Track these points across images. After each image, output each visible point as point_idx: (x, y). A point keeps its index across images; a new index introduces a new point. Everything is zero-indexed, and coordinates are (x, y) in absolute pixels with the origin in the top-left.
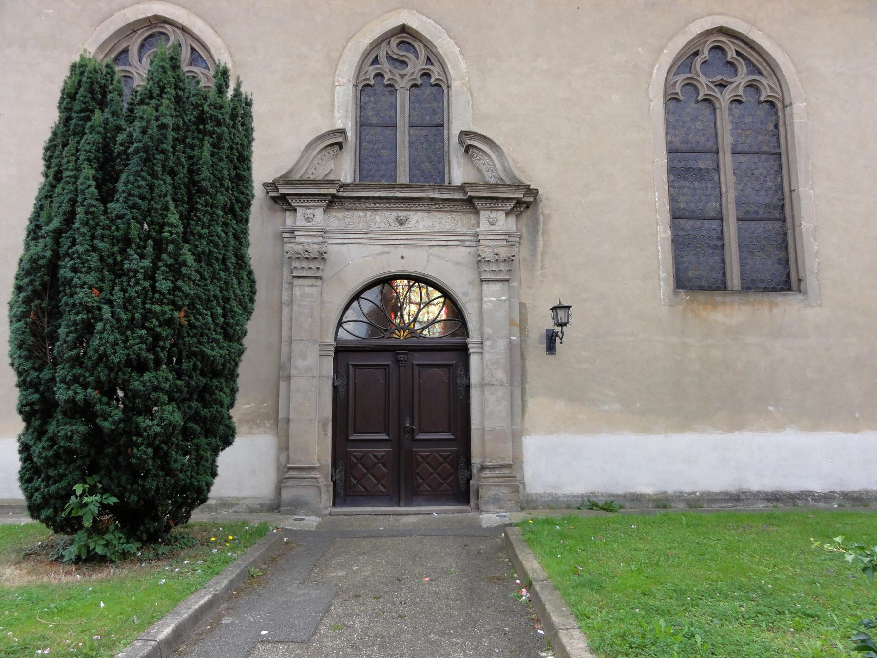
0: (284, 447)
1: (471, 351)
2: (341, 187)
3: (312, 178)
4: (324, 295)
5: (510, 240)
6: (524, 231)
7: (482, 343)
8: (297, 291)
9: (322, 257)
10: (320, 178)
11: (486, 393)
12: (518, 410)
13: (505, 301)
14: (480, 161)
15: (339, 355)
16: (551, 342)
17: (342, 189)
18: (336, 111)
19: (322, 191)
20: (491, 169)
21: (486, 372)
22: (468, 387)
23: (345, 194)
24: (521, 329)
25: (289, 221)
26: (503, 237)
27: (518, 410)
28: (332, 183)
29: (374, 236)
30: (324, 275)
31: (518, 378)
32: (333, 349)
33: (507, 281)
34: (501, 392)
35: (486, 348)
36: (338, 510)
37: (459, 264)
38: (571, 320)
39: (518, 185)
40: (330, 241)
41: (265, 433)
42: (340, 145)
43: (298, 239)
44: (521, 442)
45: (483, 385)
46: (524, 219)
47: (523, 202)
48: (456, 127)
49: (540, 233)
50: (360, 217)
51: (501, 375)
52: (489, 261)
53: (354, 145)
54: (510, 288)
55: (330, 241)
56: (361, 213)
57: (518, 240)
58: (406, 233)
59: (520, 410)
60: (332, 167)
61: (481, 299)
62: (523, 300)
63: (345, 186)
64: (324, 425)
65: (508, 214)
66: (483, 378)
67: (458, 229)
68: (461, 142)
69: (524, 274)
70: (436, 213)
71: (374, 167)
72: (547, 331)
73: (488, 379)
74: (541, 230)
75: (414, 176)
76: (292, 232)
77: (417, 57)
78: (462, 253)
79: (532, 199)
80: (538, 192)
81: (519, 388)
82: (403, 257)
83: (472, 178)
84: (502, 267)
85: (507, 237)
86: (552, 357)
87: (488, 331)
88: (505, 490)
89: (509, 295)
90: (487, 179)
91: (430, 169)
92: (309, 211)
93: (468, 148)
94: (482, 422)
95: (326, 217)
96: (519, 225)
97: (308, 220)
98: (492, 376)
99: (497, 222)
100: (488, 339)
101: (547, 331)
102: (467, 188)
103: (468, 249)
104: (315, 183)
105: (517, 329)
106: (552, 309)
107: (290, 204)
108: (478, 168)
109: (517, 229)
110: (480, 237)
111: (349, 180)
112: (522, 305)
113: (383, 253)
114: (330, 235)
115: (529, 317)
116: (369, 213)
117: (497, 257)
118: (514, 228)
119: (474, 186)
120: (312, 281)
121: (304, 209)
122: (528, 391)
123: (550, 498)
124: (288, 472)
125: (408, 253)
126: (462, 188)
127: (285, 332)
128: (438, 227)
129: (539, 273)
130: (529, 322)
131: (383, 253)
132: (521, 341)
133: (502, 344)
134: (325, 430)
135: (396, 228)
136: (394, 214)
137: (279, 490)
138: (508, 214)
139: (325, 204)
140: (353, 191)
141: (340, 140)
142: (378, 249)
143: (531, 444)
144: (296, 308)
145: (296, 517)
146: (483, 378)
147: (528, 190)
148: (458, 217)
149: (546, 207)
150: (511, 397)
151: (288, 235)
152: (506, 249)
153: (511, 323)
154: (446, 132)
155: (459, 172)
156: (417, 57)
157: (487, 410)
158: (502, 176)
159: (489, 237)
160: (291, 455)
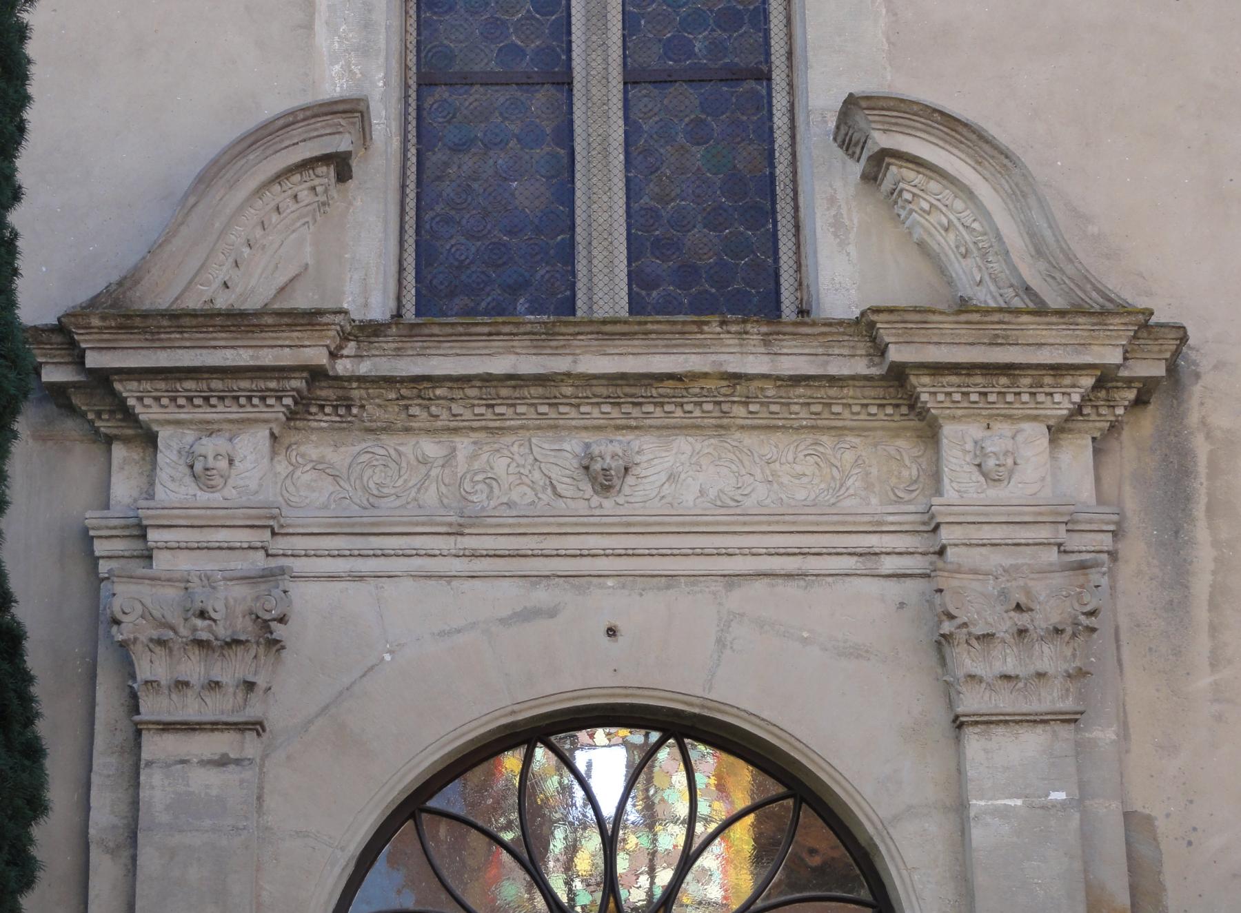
2: (345, 337)
3: (221, 303)
4: (270, 802)
5: (1074, 542)
6: (1131, 504)
9: (267, 634)
10: (252, 304)
13: (1063, 805)
14: (938, 216)
18: (320, 27)
19: (268, 358)
20: (968, 230)
25: (123, 489)
26: (1043, 533)
28: (309, 319)
30: (276, 714)
33: (1071, 719)
37: (857, 653)
39: (1100, 311)
40: (298, 565)
42: (341, 166)
43: (162, 561)
47: (1132, 381)
49: (1200, 510)
50: (424, 461)
52: (987, 638)
53: (395, 165)
54: (1082, 750)
55: (298, 565)
56: (430, 448)
57: (1106, 541)
60: (308, 254)
61: (960, 808)
62: (1138, 806)
63: (369, 332)
67: (848, 504)
68: (848, 138)
74: (1202, 500)
75: (650, 285)
76: (140, 531)
77: (1084, 614)
78: (869, 608)
79: (1159, 370)
80: (1184, 339)
82: (612, 632)
84: (1048, 658)
85: (1062, 535)
89: (1082, 785)
90: (967, 290)
91: (719, 256)
92: (210, 446)
95: (282, 467)
97: (201, 475)
102: (886, 334)
104: (238, 322)
109: (1100, 500)
110: (946, 535)
111: (378, 308)
112: (1136, 824)
114: (300, 543)
115: (1169, 879)
118: (1086, 493)
119: (915, 316)
121: (190, 436)
125: (638, 610)
126: (866, 328)
128: (759, 496)
135: (579, 498)
136: (573, 445)
138: (1057, 432)
139: (278, 412)
140: (398, 353)
141: (342, 144)
142: (508, 595)
147: (1145, 327)
148: (850, 453)
151: (118, 546)
152: (1058, 580)
154: (780, 102)
155: (844, 257)
156: (1084, 614)
158: (1031, 274)
159: (987, 533)
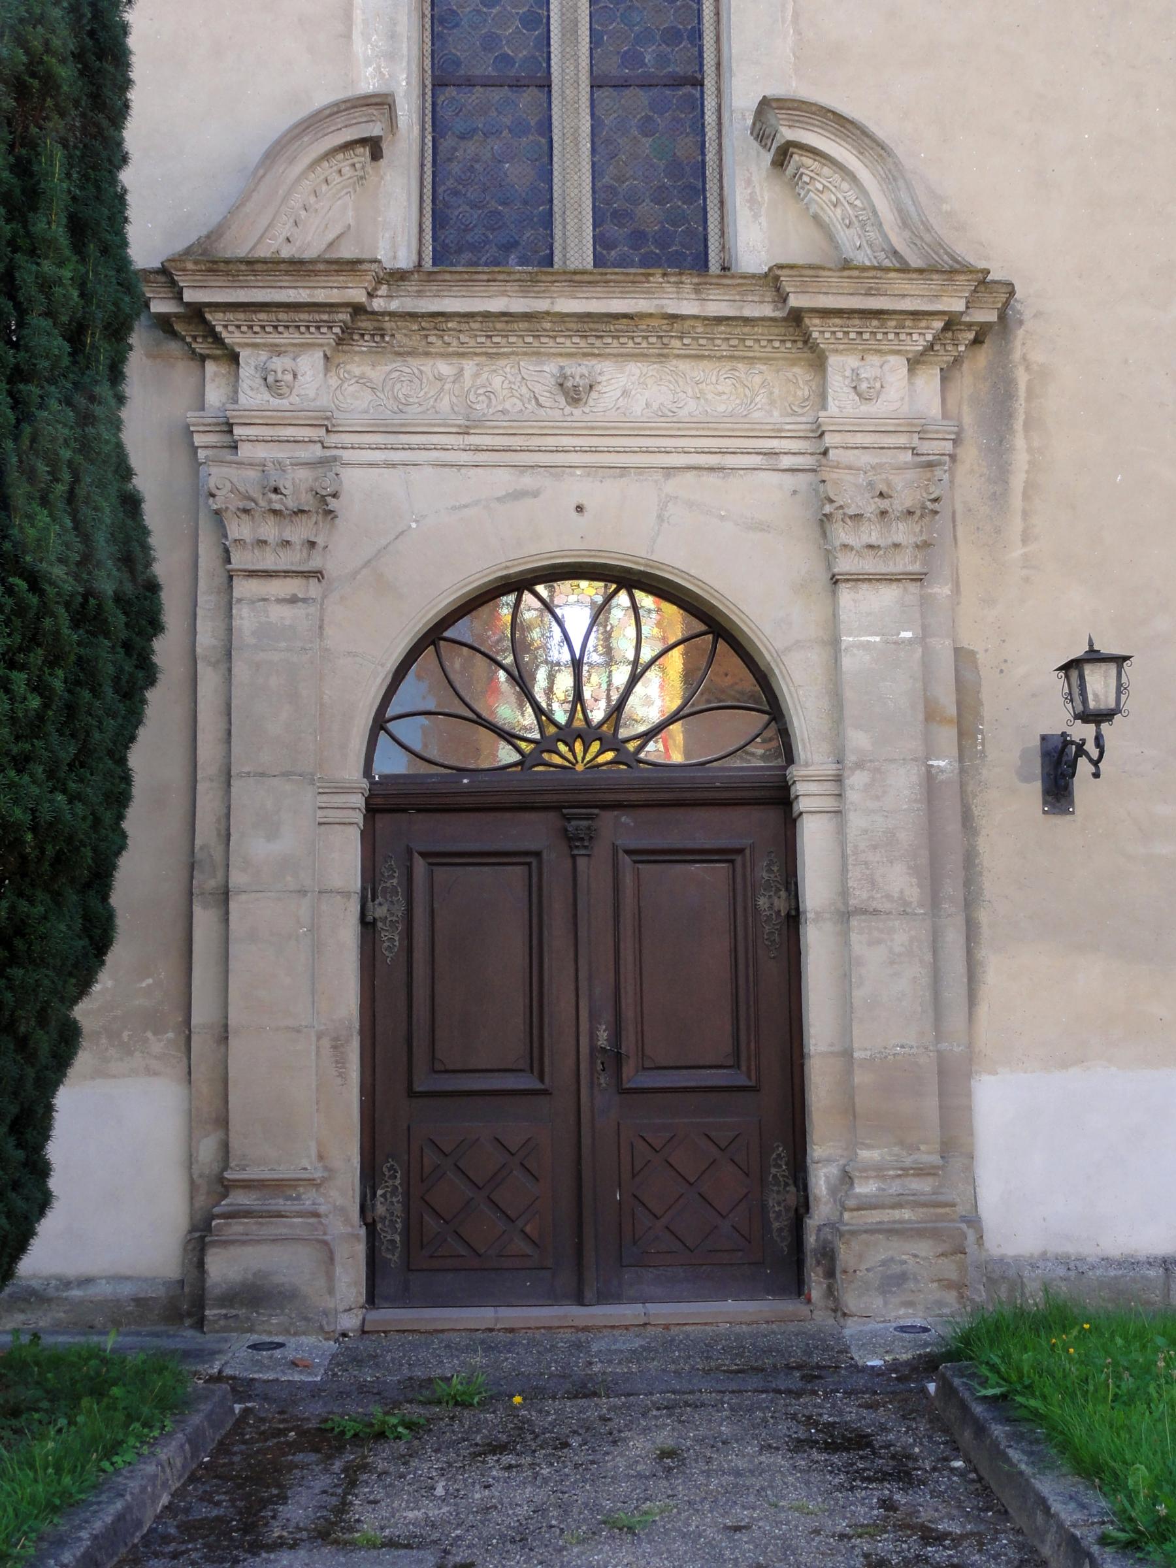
0: (214, 1114)
1: (803, 804)
2: (379, 281)
3: (285, 253)
4: (329, 631)
5: (925, 447)
6: (968, 419)
7: (838, 779)
8: (245, 620)
9: (324, 506)
11: (854, 937)
12: (955, 992)
14: (827, 194)
15: (382, 821)
16: (1059, 771)
17: (383, 290)
18: (356, 35)
19: (321, 296)
21: (854, 873)
22: (793, 919)
23: (394, 305)
24: (961, 734)
25: (215, 395)
26: (902, 440)
27: (955, 992)
28: (352, 266)
29: (487, 441)
30: (331, 568)
31: (952, 889)
32: (359, 801)
34: (901, 936)
35: (852, 796)
36: (388, 1315)
37: (762, 527)
38: (1128, 704)
39: (950, 270)
40: (347, 455)
41: (150, 1072)
42: (374, 147)
43: (245, 451)
44: (969, 1094)
45: (845, 914)
46: (967, 382)
48: (743, 85)
49: (1019, 425)
50: (440, 378)
51: (899, 881)
53: (416, 148)
54: (925, 602)
56: (445, 368)
57: (948, 447)
58: (592, 431)
59: (963, 991)
62: (968, 640)
63: (397, 277)
64: (337, 1046)
65: (915, 363)
66: (844, 893)
67: (757, 416)
68: (761, 133)
69: (968, 556)
70: (684, 366)
71: (483, 223)
72: (1044, 738)
73: (860, 895)
75: (609, 246)
78: (770, 493)
80: (1012, 293)
81: (960, 920)
82: (580, 509)
83: (798, 246)
84: (902, 533)
86: (1059, 821)
87: (858, 740)
88: (925, 1248)
89: (924, 628)
90: (849, 252)
91: (663, 226)
92: (278, 363)
93: (783, 155)
94: (846, 1030)
95: (333, 381)
96: (951, 402)
97: (272, 385)
98: (873, 883)
99: (883, 391)
100: (860, 765)
101: (1044, 738)
102: (788, 285)
103: (789, 480)
104: (298, 268)
105: (947, 736)
106: (1066, 668)
107: (218, 340)
108: (816, 218)
109: (945, 415)
110: (829, 440)
111: (404, 259)
112: (963, 657)
113: (519, 495)
114: (348, 439)
115: (985, 696)
116: (469, 366)
117: (884, 504)
120: (292, 586)
121: (263, 355)
122: (986, 932)
123: (1061, 1271)
124: (220, 1201)
126: (772, 281)
127: (208, 750)
128: (690, 408)
129: (1017, 552)
130: (987, 711)
131: (519, 495)
132: (962, 771)
133: (903, 782)
134: (341, 1062)
135: (556, 408)
136: (551, 368)
137: (201, 1237)
138: (915, 363)
140: (420, 294)
141: (375, 130)
142: (504, 480)
143: (999, 1102)
144: (241, 670)
145: (254, 1338)
146: (844, 893)
147: (982, 283)
148: (758, 376)
149: (1031, 346)
150: (935, 952)
152: (910, 475)
153: (931, 714)
154: (710, 104)
155: (757, 226)
157: (858, 995)
158: (899, 242)
159: (860, 439)
160: (234, 1143)
